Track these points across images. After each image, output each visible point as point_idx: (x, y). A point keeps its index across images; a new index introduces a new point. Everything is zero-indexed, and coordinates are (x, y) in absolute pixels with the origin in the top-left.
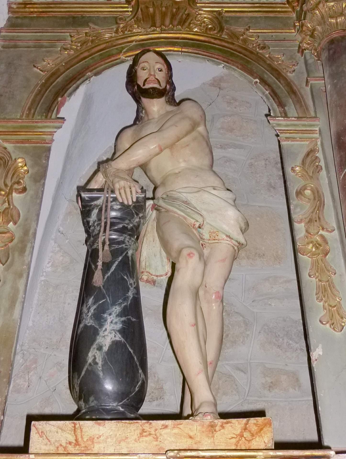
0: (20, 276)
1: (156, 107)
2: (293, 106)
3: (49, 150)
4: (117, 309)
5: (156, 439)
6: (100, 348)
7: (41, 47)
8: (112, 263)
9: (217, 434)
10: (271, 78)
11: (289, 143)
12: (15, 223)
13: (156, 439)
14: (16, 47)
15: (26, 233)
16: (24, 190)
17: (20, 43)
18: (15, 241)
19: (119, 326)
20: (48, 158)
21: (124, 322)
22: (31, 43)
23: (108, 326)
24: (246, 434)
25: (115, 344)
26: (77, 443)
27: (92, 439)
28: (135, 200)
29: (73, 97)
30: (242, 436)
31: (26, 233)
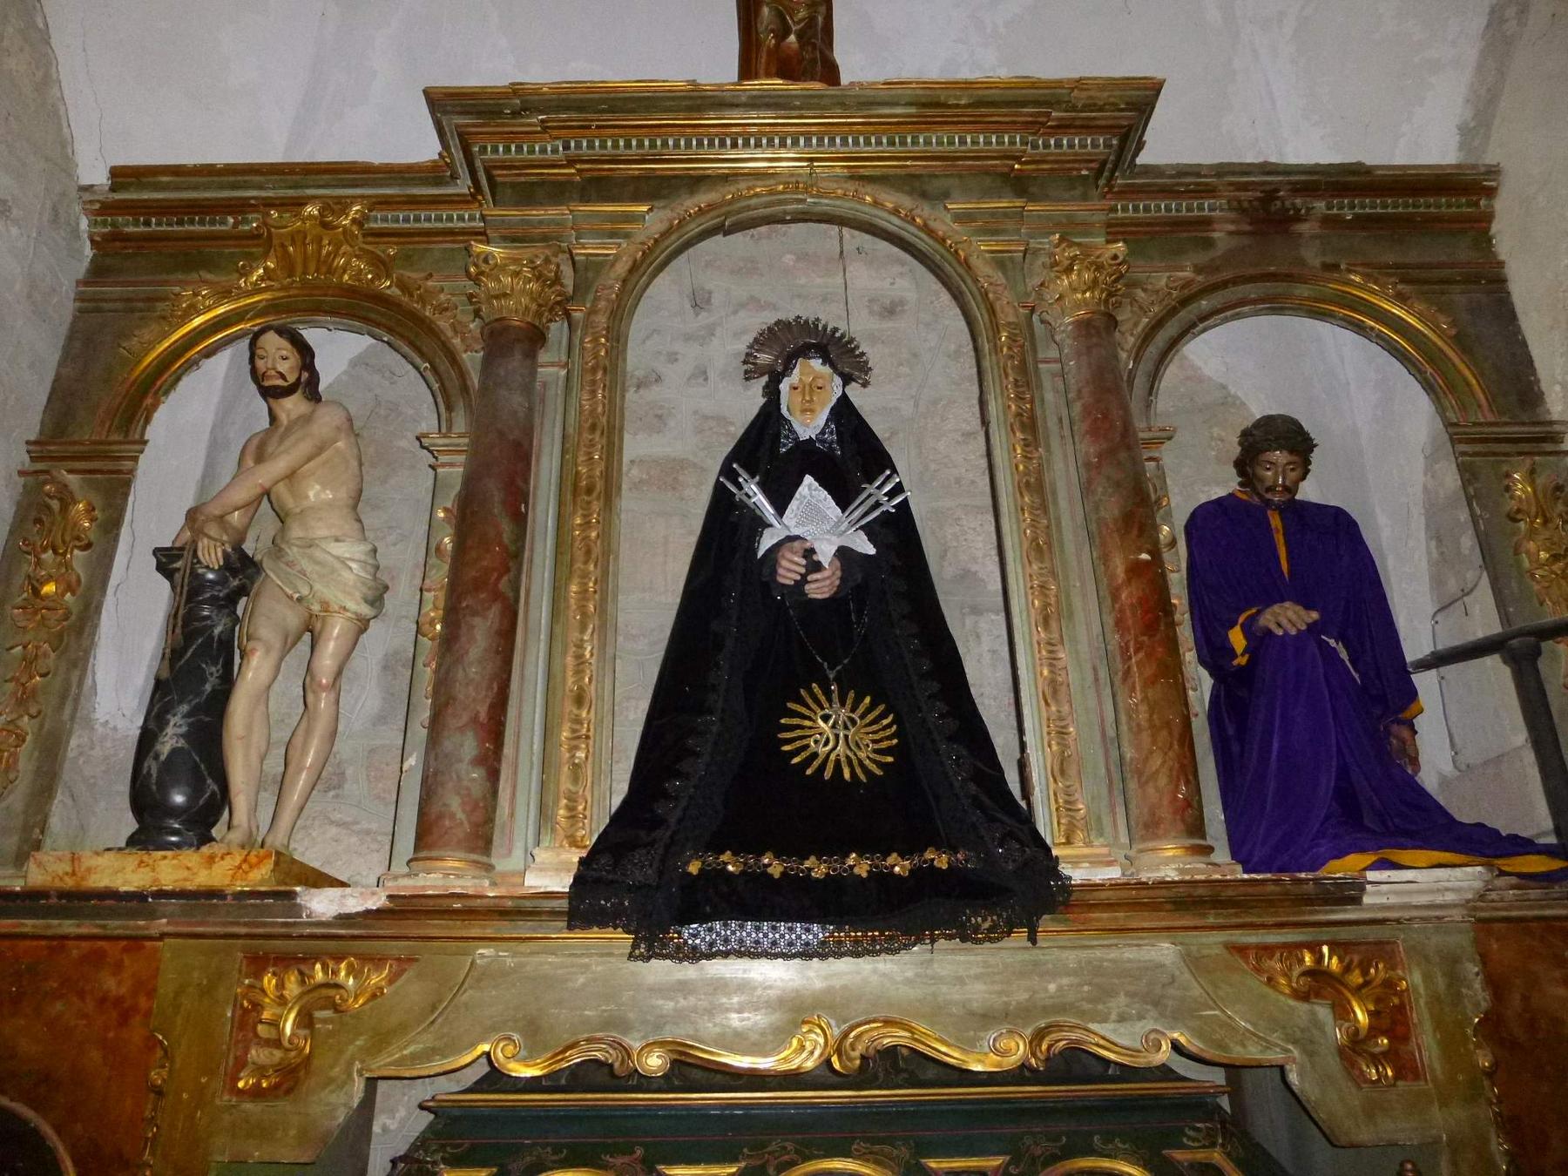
0: (75, 666)
1: (292, 406)
2: (462, 412)
3: (127, 484)
4: (185, 708)
5: (153, 870)
6: (157, 757)
7: (132, 311)
8: (185, 649)
9: (215, 867)
10: (444, 365)
11: (446, 469)
12: (73, 594)
13: (153, 870)
14: (99, 310)
15: (87, 606)
16: (88, 546)
17: (105, 305)
18: (73, 618)
19: (184, 729)
20: (126, 495)
21: (190, 725)
22: (119, 305)
23: (170, 730)
24: (245, 866)
25: (175, 752)
26: (74, 874)
27: (89, 870)
28: (1232, 215)
29: (172, 395)
30: (239, 867)
31: (87, 606)
